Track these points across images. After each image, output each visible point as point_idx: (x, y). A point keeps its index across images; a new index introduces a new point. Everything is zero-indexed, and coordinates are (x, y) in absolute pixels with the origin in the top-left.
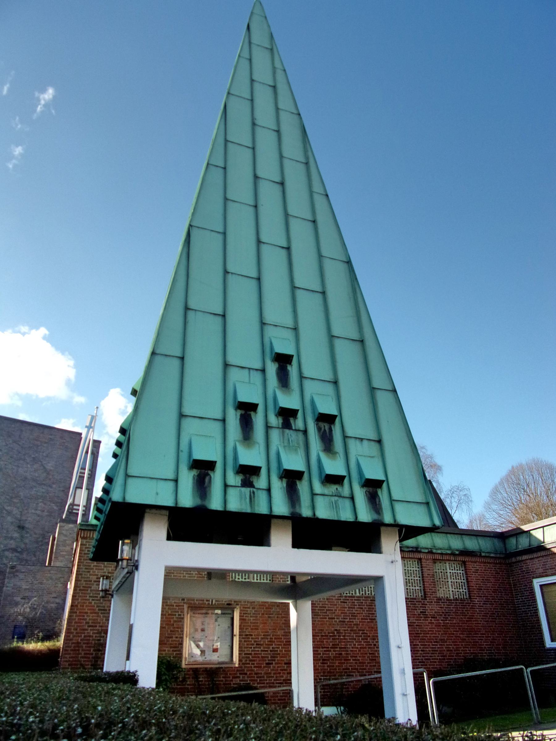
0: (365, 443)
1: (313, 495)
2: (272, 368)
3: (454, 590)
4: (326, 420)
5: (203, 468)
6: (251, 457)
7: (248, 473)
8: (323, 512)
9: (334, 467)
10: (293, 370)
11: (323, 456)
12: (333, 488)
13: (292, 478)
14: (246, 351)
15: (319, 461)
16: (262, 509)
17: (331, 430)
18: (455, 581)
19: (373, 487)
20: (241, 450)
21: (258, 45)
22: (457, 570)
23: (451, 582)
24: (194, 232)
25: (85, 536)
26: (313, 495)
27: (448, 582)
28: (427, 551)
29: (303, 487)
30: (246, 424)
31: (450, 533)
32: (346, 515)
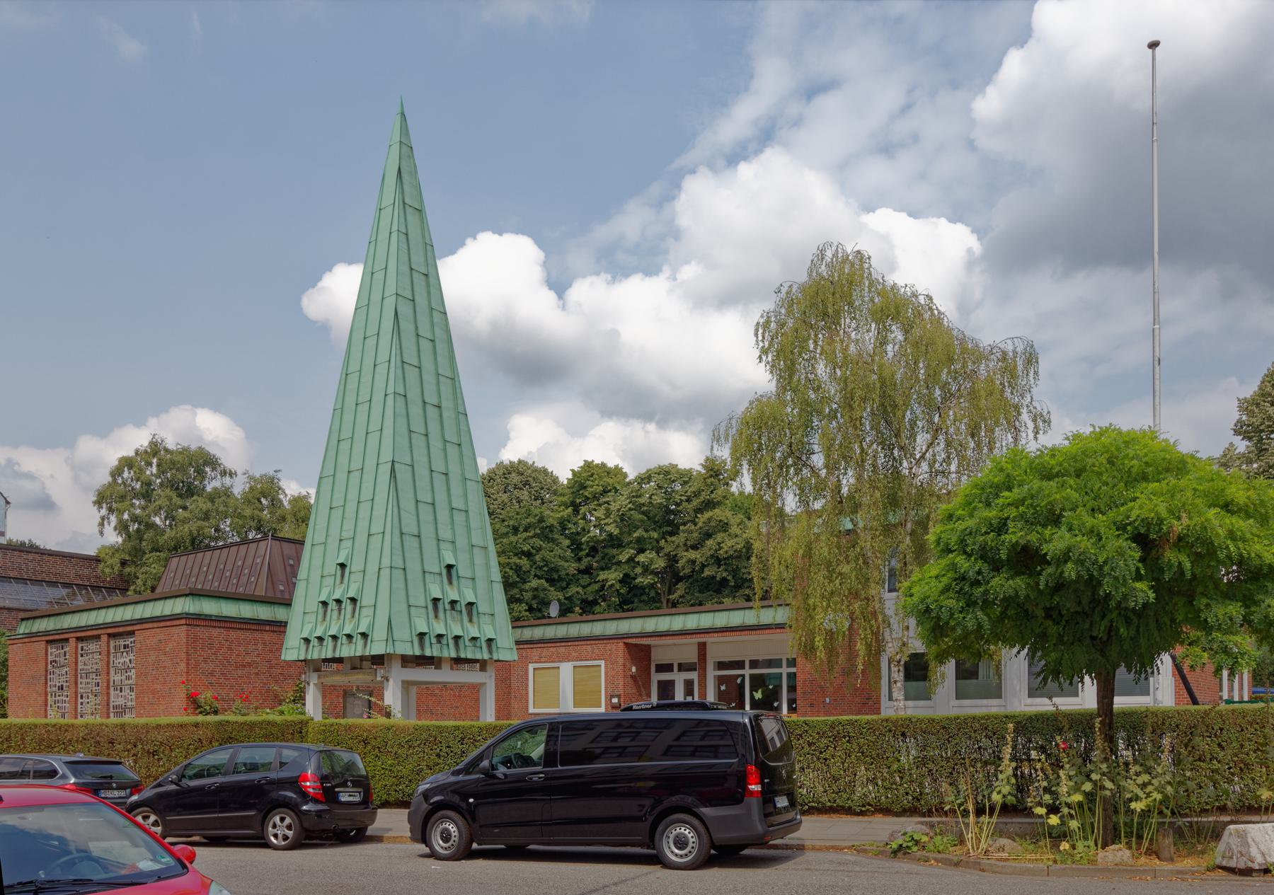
2: (444, 572)
6: (440, 629)
10: (453, 571)
24: (397, 466)
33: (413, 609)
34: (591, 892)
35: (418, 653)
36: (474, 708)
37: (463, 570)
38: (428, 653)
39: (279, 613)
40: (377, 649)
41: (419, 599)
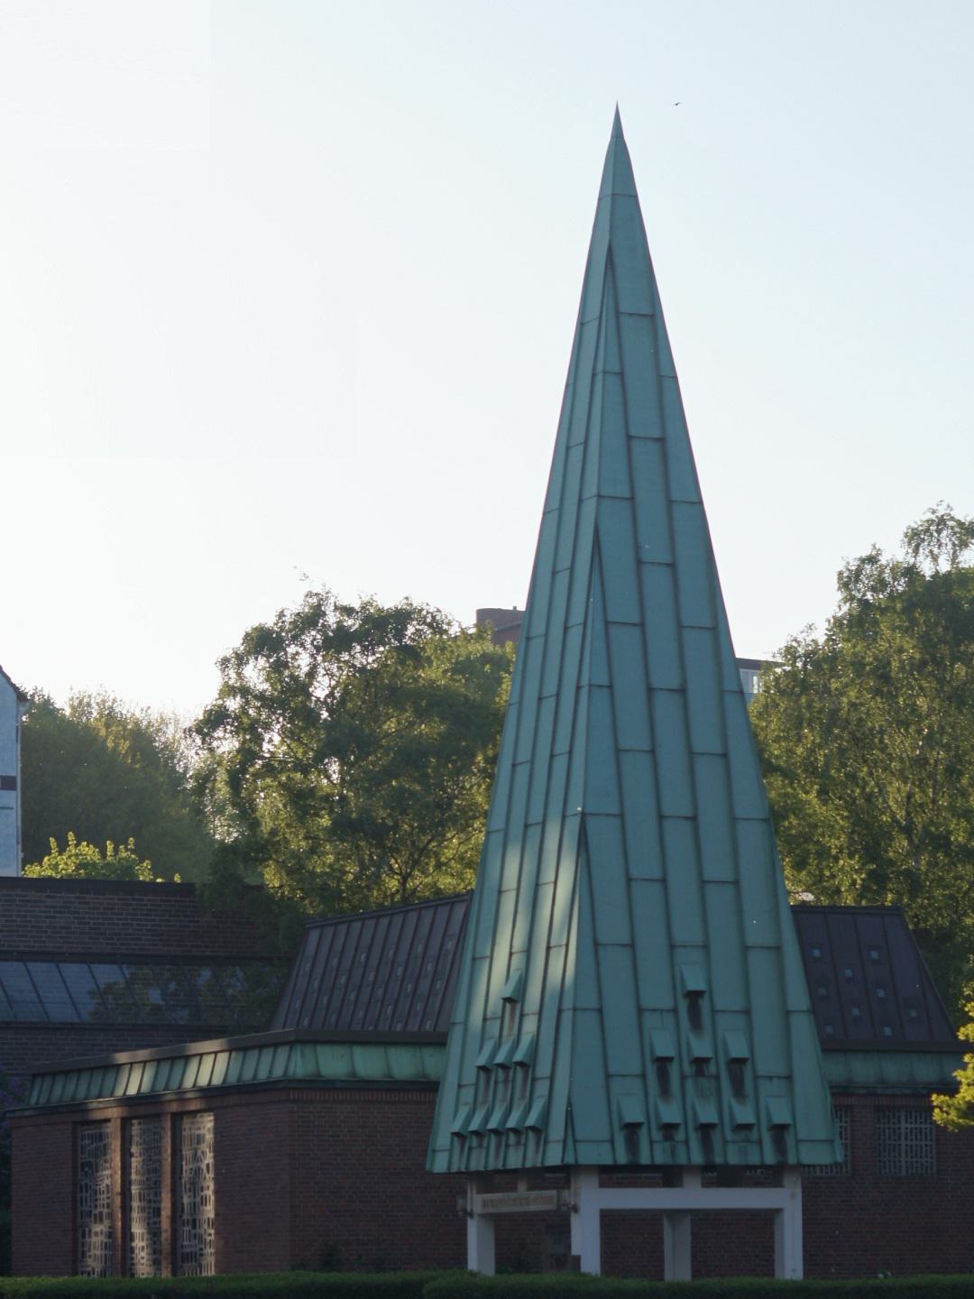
0: (775, 1080)
1: (725, 1142)
2: (683, 1005)
3: (909, 1160)
4: (737, 1064)
5: (632, 1129)
6: (671, 1113)
7: (668, 1129)
8: (733, 1159)
9: (744, 1114)
10: (704, 1004)
11: (734, 1102)
12: (743, 1134)
13: (706, 1129)
14: (658, 994)
15: (731, 1108)
16: (682, 1160)
17: (742, 1072)
18: (914, 1143)
19: (779, 1131)
20: (662, 1107)
21: (631, 314)
22: (921, 1123)
23: (907, 1145)
24: (591, 823)
25: (296, 1098)
26: (725, 1142)
27: (900, 1145)
28: (865, 1091)
29: (716, 1137)
30: (663, 1076)
31: (917, 1052)
32: (754, 1159)
33: (647, 1017)
34: (3, 986)
35: (622, 1159)
36: (766, 1255)
37: (726, 996)
38: (645, 1159)
39: (429, 1062)
40: (554, 1157)
41: (627, 1060)
